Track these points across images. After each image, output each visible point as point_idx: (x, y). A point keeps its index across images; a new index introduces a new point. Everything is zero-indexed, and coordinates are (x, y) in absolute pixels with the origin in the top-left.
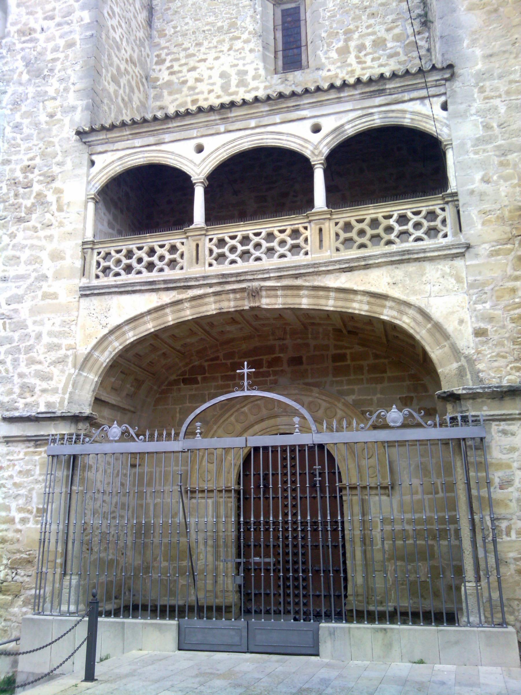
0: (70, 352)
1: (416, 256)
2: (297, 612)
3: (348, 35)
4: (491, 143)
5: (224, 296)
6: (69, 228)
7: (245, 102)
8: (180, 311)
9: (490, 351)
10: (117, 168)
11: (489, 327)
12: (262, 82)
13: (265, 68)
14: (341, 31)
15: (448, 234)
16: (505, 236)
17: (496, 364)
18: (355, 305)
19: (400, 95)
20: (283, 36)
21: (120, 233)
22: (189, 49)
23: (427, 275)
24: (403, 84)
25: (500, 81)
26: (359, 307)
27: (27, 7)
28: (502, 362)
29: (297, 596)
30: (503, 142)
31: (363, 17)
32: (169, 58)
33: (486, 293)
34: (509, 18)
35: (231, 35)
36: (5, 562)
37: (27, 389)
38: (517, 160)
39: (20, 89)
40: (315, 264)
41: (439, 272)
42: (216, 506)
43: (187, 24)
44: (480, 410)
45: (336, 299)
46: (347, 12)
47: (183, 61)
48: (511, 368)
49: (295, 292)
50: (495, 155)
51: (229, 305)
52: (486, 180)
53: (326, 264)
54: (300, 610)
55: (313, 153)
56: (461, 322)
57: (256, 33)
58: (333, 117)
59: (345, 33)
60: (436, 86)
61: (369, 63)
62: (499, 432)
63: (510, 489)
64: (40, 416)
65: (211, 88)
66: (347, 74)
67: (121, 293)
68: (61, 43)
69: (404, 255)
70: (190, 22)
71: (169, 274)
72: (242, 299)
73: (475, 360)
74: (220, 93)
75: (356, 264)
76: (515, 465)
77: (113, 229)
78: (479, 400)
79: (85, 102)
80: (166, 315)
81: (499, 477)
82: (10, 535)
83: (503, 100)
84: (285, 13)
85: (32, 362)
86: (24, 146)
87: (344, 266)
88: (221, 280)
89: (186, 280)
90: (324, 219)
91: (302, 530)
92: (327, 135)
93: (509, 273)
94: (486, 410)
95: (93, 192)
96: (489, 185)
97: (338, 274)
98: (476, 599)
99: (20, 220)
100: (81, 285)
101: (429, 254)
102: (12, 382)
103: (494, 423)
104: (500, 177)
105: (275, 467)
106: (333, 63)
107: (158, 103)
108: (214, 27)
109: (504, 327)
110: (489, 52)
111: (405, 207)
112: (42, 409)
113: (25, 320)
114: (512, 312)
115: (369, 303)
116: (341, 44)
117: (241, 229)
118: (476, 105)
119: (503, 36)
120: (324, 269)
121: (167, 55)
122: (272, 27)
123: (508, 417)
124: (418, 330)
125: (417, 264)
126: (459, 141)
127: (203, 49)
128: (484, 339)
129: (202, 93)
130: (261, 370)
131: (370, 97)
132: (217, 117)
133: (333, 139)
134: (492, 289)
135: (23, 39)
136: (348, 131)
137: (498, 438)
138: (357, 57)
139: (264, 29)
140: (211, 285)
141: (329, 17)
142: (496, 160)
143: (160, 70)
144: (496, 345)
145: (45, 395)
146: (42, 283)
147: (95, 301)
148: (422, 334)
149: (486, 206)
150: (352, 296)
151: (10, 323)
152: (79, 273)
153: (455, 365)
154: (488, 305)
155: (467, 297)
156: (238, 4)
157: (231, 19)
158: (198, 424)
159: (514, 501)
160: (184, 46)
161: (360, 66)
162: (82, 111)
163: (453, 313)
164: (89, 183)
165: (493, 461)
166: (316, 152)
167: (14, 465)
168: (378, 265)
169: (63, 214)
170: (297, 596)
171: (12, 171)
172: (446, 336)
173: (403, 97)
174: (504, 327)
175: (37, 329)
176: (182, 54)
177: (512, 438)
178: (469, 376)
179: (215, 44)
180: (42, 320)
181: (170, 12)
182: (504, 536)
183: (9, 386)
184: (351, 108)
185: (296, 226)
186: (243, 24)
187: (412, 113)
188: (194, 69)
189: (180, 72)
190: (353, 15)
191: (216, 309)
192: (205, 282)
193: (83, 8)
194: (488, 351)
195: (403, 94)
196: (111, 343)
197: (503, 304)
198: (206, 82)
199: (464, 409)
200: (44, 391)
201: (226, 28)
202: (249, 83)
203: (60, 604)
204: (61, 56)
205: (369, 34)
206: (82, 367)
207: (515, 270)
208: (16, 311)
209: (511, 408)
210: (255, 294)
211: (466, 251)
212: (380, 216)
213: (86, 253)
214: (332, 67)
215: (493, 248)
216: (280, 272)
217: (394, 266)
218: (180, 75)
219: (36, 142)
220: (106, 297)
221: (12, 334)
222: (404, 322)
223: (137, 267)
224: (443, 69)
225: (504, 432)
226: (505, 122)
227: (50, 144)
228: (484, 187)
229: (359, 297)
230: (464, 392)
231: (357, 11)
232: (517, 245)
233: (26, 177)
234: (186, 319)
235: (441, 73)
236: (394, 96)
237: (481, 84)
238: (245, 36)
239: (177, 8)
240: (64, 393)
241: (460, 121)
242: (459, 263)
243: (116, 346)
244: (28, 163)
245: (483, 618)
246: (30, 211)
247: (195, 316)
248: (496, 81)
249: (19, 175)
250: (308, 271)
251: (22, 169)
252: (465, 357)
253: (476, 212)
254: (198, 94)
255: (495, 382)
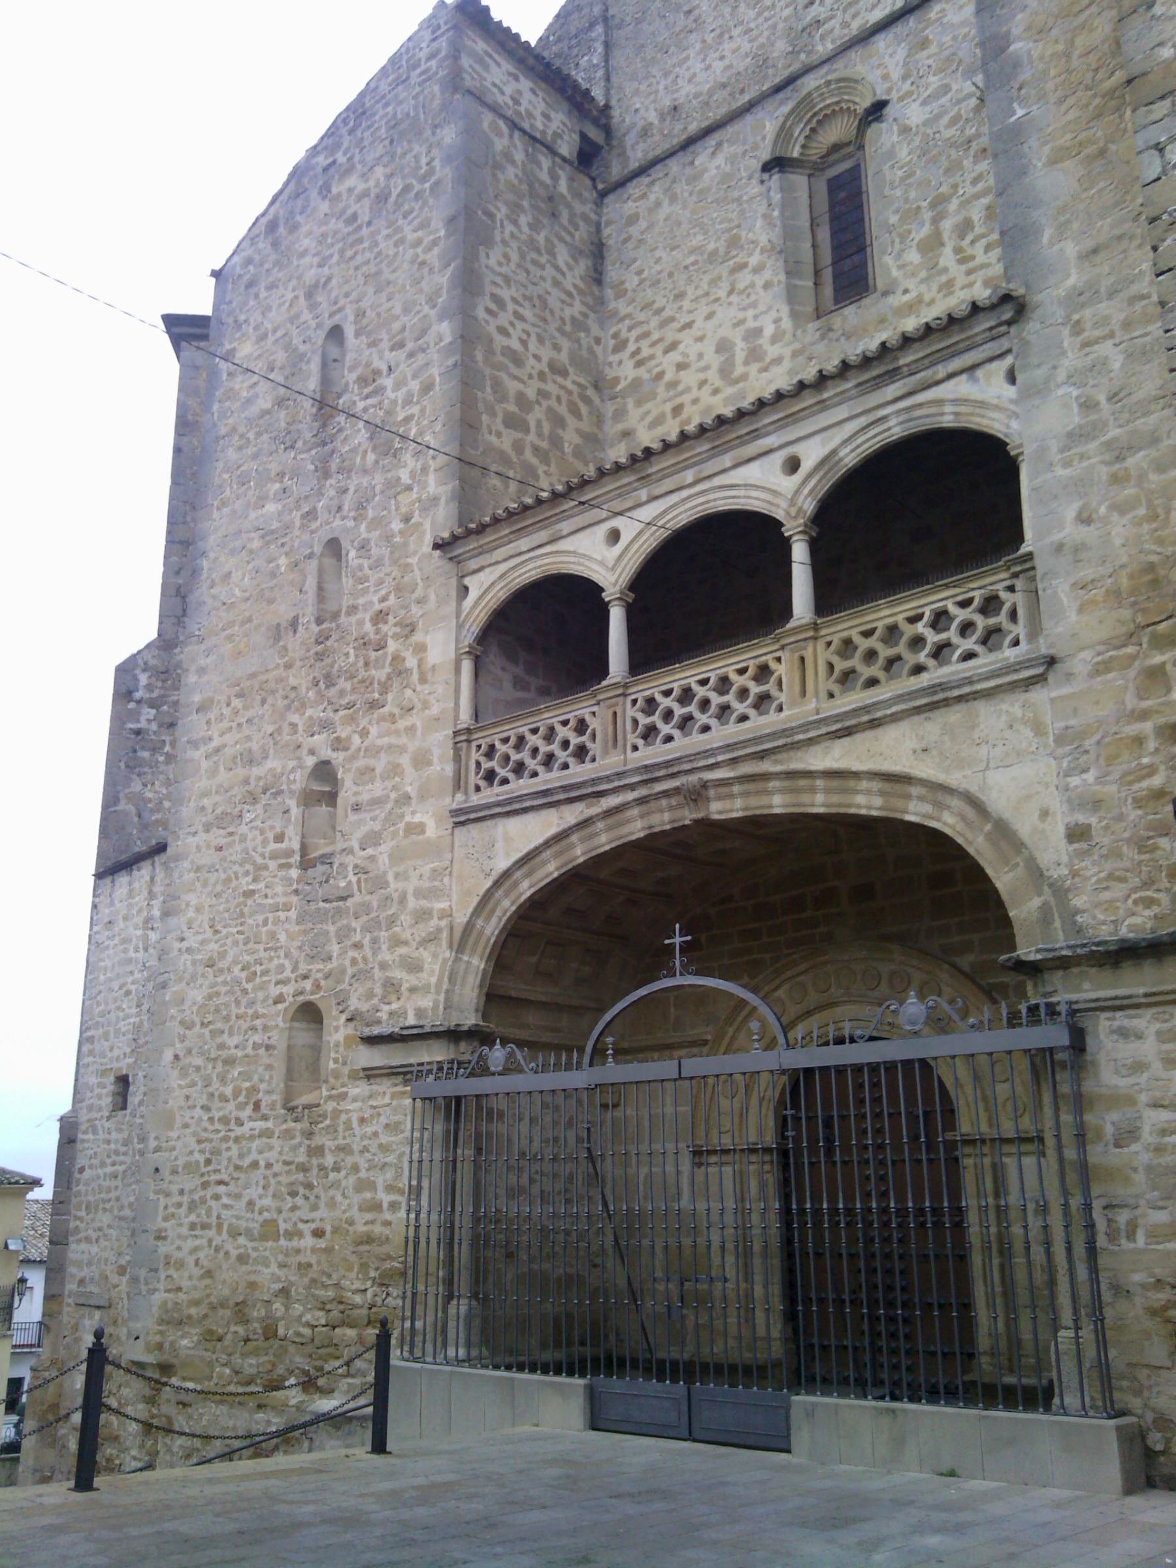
0: (443, 923)
1: (956, 693)
2: (896, 1384)
3: (939, 208)
4: (1095, 438)
5: (653, 805)
6: (435, 710)
7: (667, 446)
8: (591, 836)
9: (1096, 869)
10: (500, 594)
11: (1093, 820)
12: (788, 344)
13: (794, 315)
14: (925, 204)
15: (1021, 637)
16: (1124, 629)
17: (1106, 895)
18: (860, 799)
19: (929, 372)
20: (834, 234)
21: (544, 692)
22: (663, 309)
23: (982, 727)
24: (929, 351)
25: (1111, 303)
26: (867, 802)
27: (368, 335)
28: (1118, 891)
29: (894, 1352)
30: (1118, 431)
31: (965, 162)
32: (634, 334)
33: (1086, 752)
34: (1128, 162)
35: (731, 263)
36: (372, 1274)
37: (392, 987)
38: (1145, 465)
39: (365, 481)
40: (785, 730)
41: (1004, 718)
42: (741, 1179)
43: (658, 260)
44: (1078, 989)
45: (827, 791)
46: (934, 160)
47: (655, 336)
48: (1135, 902)
49: (760, 785)
50: (1102, 462)
51: (663, 819)
52: (1084, 519)
53: (805, 727)
54: (900, 1379)
55: (788, 513)
56: (1045, 814)
57: (773, 248)
58: (817, 439)
59: (933, 206)
60: (993, 339)
61: (981, 258)
62: (1113, 1032)
63: (1134, 1147)
64: (405, 1032)
65: (702, 376)
66: (940, 291)
67: (508, 814)
68: (415, 386)
69: (935, 693)
70: (664, 255)
71: (579, 772)
72: (680, 806)
73: (1068, 890)
74: (718, 383)
75: (853, 722)
76: (1143, 1098)
77: (525, 687)
78: (1075, 970)
79: (449, 487)
80: (572, 846)
81: (1113, 1123)
82: (378, 1229)
83: (1117, 341)
84: (834, 185)
85: (397, 942)
86: (374, 577)
87: (834, 728)
88: (645, 777)
89: (594, 781)
90: (805, 639)
91: (900, 1225)
92: (809, 476)
93: (1129, 706)
94: (1087, 989)
95: (469, 638)
96: (1091, 528)
97: (828, 743)
98: (1075, 1362)
99: (373, 705)
100: (454, 806)
101: (978, 687)
102: (372, 978)
103: (1104, 1015)
104: (1113, 507)
105: (843, 1104)
106: (913, 275)
107: (620, 427)
108: (702, 254)
109: (1120, 818)
110: (1089, 244)
111: (940, 597)
112: (411, 1020)
113: (385, 873)
114: (1136, 787)
115: (882, 793)
116: (926, 230)
117: (677, 676)
118: (1066, 363)
119: (1116, 204)
120: (801, 737)
121: (630, 329)
122: (808, 224)
123: (1125, 1002)
124: (970, 836)
125: (962, 707)
126: (1034, 446)
127: (686, 304)
128: (1083, 845)
129: (688, 390)
130: (804, 915)
131: (877, 387)
132: (633, 478)
133: (819, 481)
134: (1099, 742)
135: (366, 391)
136: (846, 460)
137: (1110, 1046)
138: (958, 250)
139: (789, 233)
140: (632, 787)
141: (903, 179)
142: (1104, 472)
143: (620, 362)
144: (1105, 857)
145: (414, 996)
146: (404, 809)
147: (474, 830)
148: (977, 844)
149: (1087, 573)
150: (852, 783)
151: (366, 880)
152: (450, 788)
153: (1036, 902)
154: (1090, 777)
155: (1053, 763)
156: (741, 197)
157: (729, 230)
158: (610, 1040)
159: (1140, 1169)
160: (655, 306)
161: (963, 268)
162: (447, 502)
163: (1028, 797)
164: (460, 627)
165: (1104, 1091)
166: (793, 511)
167: (379, 1115)
168: (895, 718)
169: (426, 688)
170: (894, 1352)
171: (361, 623)
172: (1018, 845)
173: (935, 373)
174: (1120, 818)
175: (400, 885)
176: (655, 322)
177: (1137, 1044)
178: (1057, 924)
179: (706, 287)
180: (406, 872)
181: (630, 245)
182: (1123, 1241)
183: (369, 984)
184: (846, 415)
185: (763, 658)
186: (750, 235)
187: (955, 401)
188: (673, 346)
189: (652, 357)
190: (946, 164)
191: (643, 829)
192: (622, 783)
193: (441, 318)
194: (1092, 870)
195: (935, 368)
196: (498, 902)
197: (1117, 770)
198: (694, 367)
199: (1049, 989)
200: (413, 990)
201: (722, 251)
202: (766, 353)
203: (445, 1345)
204: (415, 410)
205: (977, 197)
206: (461, 949)
207: (1141, 698)
208: (372, 858)
209: (1135, 982)
210: (697, 795)
211: (1047, 669)
212: (900, 618)
213: (460, 749)
214: (911, 284)
215: (1100, 658)
216: (732, 751)
217: (923, 716)
218: (653, 363)
219: (388, 570)
220: (489, 823)
221: (368, 898)
222: (945, 824)
223: (531, 764)
224: (993, 307)
225: (1123, 1033)
226: (1121, 389)
227: (407, 568)
228: (1087, 534)
229: (864, 784)
230: (1039, 957)
231: (953, 152)
232: (1145, 646)
233: (377, 632)
234: (602, 850)
235: (994, 314)
236: (918, 376)
237: (1076, 317)
238: (754, 260)
239: (642, 233)
240: (438, 993)
241: (1036, 402)
242: (1039, 696)
243: (507, 906)
244: (378, 607)
245: (1087, 1399)
246: (384, 689)
247: (614, 845)
248: (1104, 305)
249: (368, 627)
250: (776, 744)
251: (372, 619)
252: (1051, 885)
253: (1067, 588)
254: (682, 393)
255: (1105, 933)
